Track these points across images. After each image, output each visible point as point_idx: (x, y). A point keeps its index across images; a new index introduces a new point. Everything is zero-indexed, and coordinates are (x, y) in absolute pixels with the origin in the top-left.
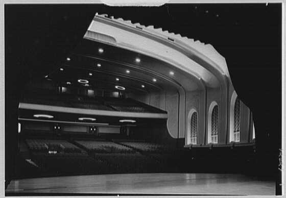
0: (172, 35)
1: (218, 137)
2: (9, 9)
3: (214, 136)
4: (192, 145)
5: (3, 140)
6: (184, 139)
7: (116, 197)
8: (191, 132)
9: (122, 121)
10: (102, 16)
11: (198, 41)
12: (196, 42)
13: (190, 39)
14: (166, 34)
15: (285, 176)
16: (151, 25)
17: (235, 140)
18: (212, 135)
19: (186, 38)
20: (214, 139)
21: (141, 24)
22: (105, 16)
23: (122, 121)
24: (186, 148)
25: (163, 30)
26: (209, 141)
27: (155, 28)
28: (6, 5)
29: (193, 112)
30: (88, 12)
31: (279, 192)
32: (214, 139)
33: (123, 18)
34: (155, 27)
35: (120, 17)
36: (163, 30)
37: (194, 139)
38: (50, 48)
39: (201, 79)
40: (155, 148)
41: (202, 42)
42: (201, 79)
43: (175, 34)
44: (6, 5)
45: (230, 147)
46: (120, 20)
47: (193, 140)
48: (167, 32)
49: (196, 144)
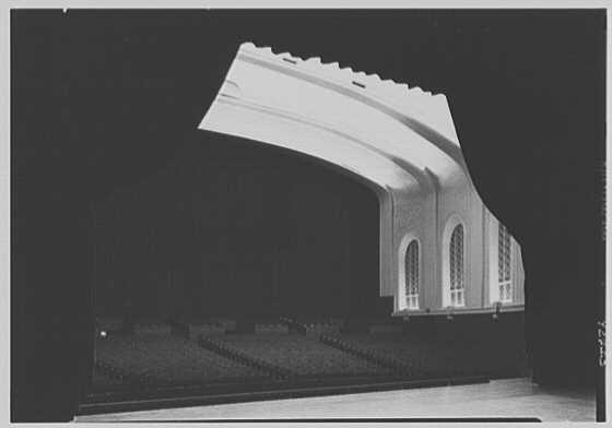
1: (465, 293)
2: (19, 18)
3: (505, 283)
4: (454, 309)
6: (392, 298)
8: (407, 284)
11: (376, 76)
12: (412, 90)
17: (502, 299)
18: (407, 294)
19: (391, 81)
20: (456, 297)
21: (293, 55)
24: (395, 318)
26: (447, 302)
27: (323, 62)
28: (13, 12)
29: (410, 240)
30: (216, 39)
31: (601, 417)
32: (456, 297)
33: (379, 75)
34: (354, 70)
35: (249, 41)
36: (341, 67)
37: (414, 299)
38: (115, 102)
39: (426, 169)
40: (330, 325)
41: (424, 90)
42: (426, 169)
44: (13, 12)
45: (491, 314)
47: (411, 301)
49: (417, 308)
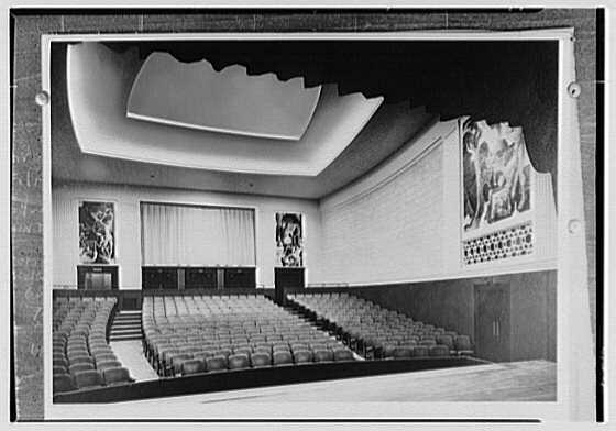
7: (394, 7)
27: (249, 73)
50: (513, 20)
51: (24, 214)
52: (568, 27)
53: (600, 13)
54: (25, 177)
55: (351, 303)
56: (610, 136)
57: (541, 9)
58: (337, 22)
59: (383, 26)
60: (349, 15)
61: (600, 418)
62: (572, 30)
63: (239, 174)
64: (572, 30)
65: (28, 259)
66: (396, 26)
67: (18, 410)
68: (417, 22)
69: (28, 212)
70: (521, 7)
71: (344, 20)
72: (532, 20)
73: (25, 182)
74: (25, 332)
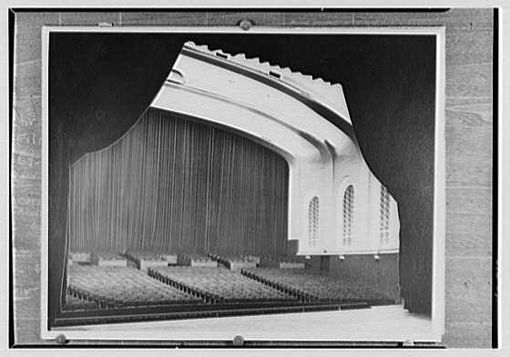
0: (276, 69)
5: (490, 50)
7: (327, 7)
9: (77, 311)
10: (214, 53)
11: (320, 80)
12: (50, 332)
13: (307, 76)
14: (265, 68)
15: (503, 176)
16: (240, 52)
19: (300, 73)
22: (217, 54)
23: (77, 311)
25: (261, 61)
27: (247, 57)
33: (195, 42)
36: (261, 61)
41: (325, 80)
43: (293, 71)
46: (240, 60)
48: (268, 64)
50: (294, 18)
51: (31, 165)
52: (441, 26)
53: (496, 11)
54: (32, 136)
55: (134, 297)
56: (503, 113)
57: (448, 9)
58: (269, 20)
59: (305, 23)
60: (279, 14)
61: (495, 345)
62: (444, 28)
63: (324, 117)
64: (444, 28)
65: (33, 200)
66: (315, 23)
67: (15, 313)
68: (330, 20)
69: (33, 164)
70: (323, 7)
71: (275, 19)
72: (418, 18)
73: (31, 141)
74: (31, 256)
